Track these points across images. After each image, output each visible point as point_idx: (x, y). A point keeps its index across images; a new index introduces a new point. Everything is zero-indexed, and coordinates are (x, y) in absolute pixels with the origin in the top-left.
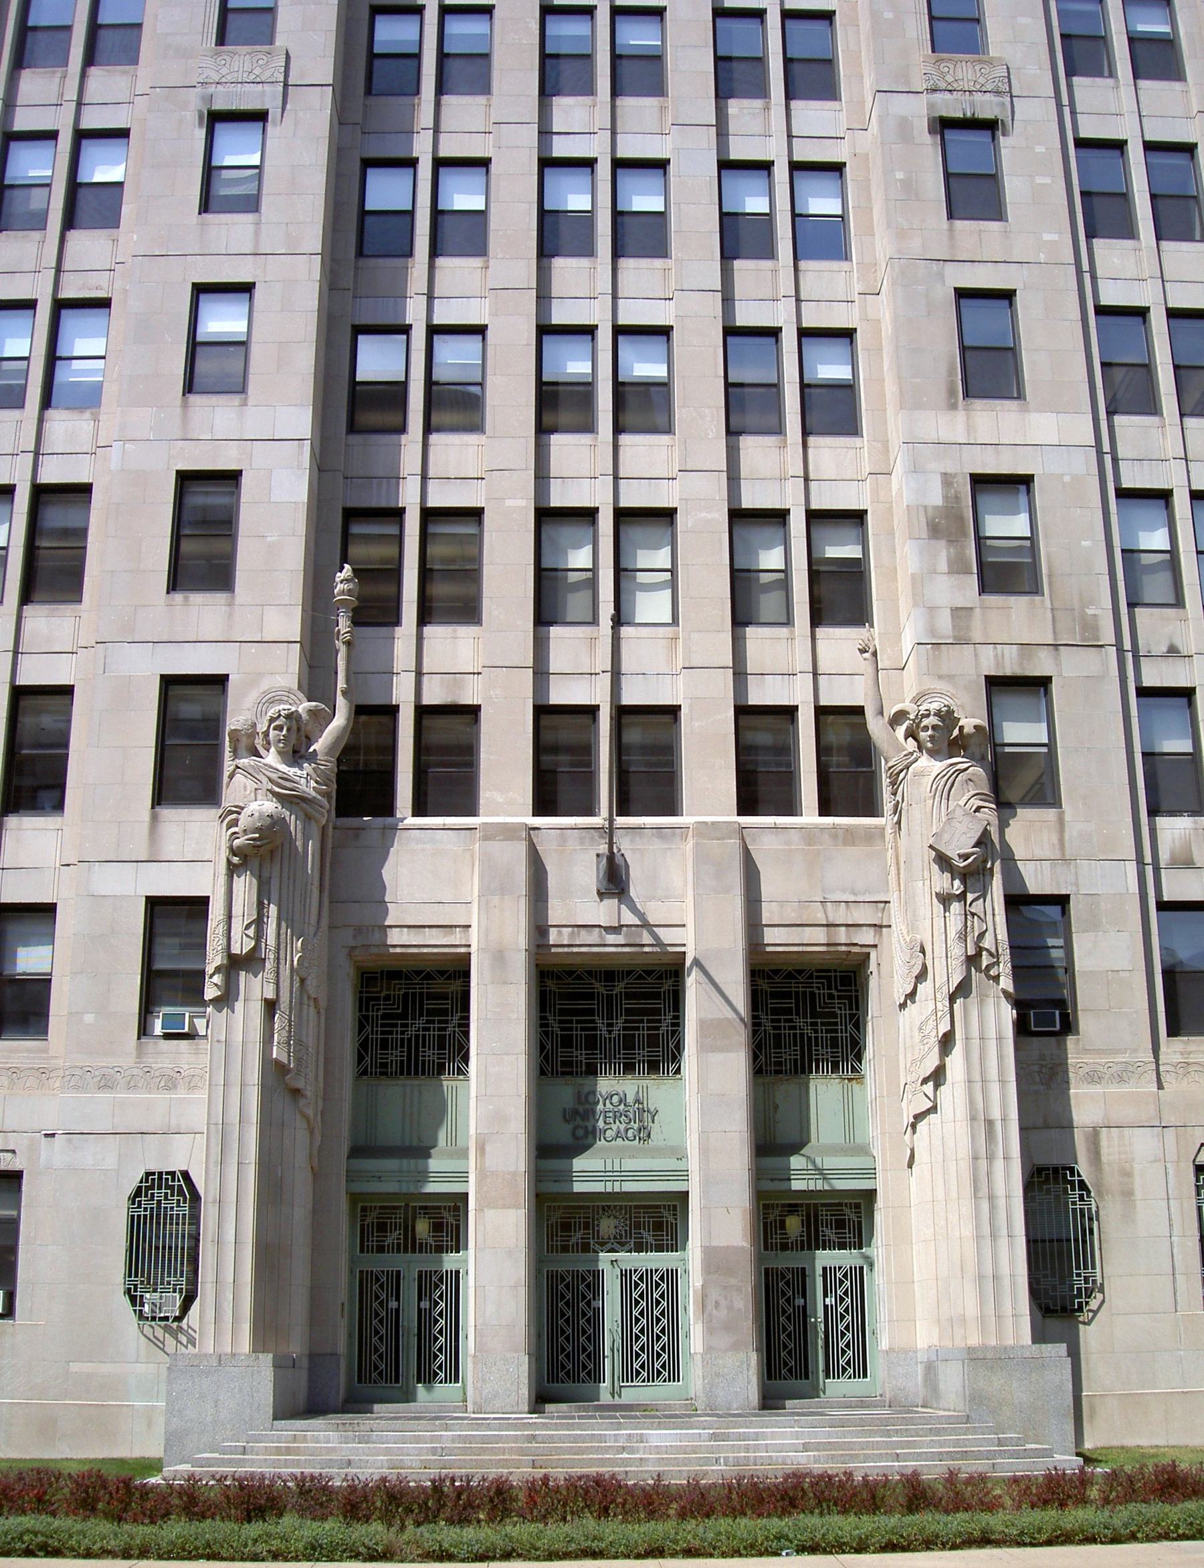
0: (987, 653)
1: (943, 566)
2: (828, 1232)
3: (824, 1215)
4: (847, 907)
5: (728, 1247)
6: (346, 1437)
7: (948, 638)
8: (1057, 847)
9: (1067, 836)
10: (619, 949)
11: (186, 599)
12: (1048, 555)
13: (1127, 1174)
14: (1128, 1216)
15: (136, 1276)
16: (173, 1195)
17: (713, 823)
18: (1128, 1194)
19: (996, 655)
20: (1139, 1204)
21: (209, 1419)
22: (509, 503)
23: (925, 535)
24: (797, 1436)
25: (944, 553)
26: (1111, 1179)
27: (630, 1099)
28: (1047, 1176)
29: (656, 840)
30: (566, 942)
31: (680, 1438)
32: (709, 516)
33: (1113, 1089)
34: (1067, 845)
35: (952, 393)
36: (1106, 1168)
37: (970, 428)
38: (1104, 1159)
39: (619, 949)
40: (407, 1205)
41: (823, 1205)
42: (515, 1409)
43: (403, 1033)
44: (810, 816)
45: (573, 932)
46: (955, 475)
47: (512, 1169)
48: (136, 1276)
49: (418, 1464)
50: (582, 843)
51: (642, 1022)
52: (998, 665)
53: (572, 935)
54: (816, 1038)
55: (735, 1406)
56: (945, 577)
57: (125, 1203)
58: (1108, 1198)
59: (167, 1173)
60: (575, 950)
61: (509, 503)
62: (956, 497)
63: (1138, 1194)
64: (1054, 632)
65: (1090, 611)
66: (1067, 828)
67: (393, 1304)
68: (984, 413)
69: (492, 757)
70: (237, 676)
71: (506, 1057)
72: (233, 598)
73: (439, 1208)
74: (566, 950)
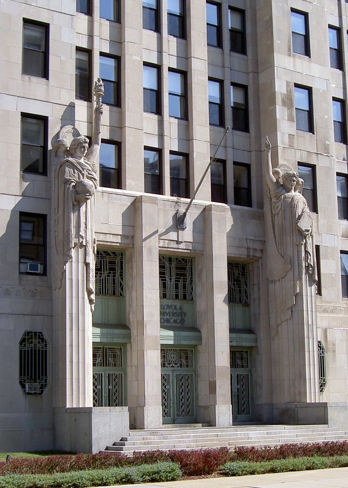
0: (298, 153)
1: (286, 118)
2: (238, 361)
3: (109, 353)
4: (253, 242)
5: (223, 366)
6: (160, 438)
7: (287, 145)
8: (317, 227)
9: (319, 224)
10: (183, 251)
11: (30, 78)
12: (315, 118)
13: (334, 345)
14: (334, 359)
15: (25, 375)
16: (321, 349)
17: (217, 206)
18: (334, 351)
19: (301, 154)
20: (337, 355)
21: (108, 433)
22: (134, 57)
23: (281, 104)
24: (259, 434)
25: (286, 112)
26: (330, 347)
27: (178, 308)
28: (32, 335)
29: (195, 209)
30: (166, 246)
31: (259, 434)
32: (202, 78)
33: (331, 315)
34: (319, 227)
35: (289, 49)
36: (328, 342)
37: (294, 65)
38: (328, 339)
39: (183, 251)
40: (103, 348)
41: (237, 351)
42: (158, 427)
43: (100, 277)
44: (167, 196)
45: (169, 242)
46: (290, 83)
47: (156, 335)
48: (25, 375)
49: (195, 446)
50: (171, 207)
51: (181, 278)
52: (301, 158)
53: (168, 243)
54: (235, 289)
55: (226, 425)
56: (287, 122)
57: (18, 345)
58: (329, 352)
59: (39, 333)
60: (169, 249)
61: (134, 57)
62: (290, 91)
63: (337, 352)
64: (317, 149)
65: (327, 142)
66: (319, 222)
67: (110, 387)
68: (299, 60)
69: (130, 166)
70: (51, 118)
71: (152, 291)
72: (49, 82)
73: (187, 350)
74: (166, 249)
